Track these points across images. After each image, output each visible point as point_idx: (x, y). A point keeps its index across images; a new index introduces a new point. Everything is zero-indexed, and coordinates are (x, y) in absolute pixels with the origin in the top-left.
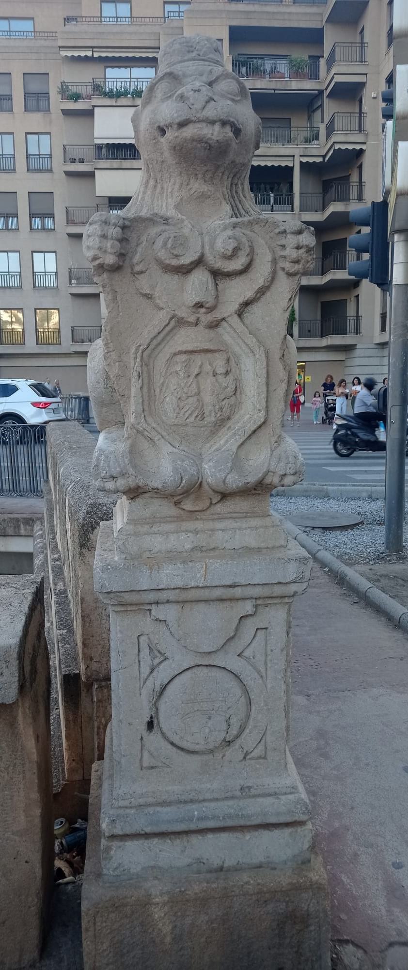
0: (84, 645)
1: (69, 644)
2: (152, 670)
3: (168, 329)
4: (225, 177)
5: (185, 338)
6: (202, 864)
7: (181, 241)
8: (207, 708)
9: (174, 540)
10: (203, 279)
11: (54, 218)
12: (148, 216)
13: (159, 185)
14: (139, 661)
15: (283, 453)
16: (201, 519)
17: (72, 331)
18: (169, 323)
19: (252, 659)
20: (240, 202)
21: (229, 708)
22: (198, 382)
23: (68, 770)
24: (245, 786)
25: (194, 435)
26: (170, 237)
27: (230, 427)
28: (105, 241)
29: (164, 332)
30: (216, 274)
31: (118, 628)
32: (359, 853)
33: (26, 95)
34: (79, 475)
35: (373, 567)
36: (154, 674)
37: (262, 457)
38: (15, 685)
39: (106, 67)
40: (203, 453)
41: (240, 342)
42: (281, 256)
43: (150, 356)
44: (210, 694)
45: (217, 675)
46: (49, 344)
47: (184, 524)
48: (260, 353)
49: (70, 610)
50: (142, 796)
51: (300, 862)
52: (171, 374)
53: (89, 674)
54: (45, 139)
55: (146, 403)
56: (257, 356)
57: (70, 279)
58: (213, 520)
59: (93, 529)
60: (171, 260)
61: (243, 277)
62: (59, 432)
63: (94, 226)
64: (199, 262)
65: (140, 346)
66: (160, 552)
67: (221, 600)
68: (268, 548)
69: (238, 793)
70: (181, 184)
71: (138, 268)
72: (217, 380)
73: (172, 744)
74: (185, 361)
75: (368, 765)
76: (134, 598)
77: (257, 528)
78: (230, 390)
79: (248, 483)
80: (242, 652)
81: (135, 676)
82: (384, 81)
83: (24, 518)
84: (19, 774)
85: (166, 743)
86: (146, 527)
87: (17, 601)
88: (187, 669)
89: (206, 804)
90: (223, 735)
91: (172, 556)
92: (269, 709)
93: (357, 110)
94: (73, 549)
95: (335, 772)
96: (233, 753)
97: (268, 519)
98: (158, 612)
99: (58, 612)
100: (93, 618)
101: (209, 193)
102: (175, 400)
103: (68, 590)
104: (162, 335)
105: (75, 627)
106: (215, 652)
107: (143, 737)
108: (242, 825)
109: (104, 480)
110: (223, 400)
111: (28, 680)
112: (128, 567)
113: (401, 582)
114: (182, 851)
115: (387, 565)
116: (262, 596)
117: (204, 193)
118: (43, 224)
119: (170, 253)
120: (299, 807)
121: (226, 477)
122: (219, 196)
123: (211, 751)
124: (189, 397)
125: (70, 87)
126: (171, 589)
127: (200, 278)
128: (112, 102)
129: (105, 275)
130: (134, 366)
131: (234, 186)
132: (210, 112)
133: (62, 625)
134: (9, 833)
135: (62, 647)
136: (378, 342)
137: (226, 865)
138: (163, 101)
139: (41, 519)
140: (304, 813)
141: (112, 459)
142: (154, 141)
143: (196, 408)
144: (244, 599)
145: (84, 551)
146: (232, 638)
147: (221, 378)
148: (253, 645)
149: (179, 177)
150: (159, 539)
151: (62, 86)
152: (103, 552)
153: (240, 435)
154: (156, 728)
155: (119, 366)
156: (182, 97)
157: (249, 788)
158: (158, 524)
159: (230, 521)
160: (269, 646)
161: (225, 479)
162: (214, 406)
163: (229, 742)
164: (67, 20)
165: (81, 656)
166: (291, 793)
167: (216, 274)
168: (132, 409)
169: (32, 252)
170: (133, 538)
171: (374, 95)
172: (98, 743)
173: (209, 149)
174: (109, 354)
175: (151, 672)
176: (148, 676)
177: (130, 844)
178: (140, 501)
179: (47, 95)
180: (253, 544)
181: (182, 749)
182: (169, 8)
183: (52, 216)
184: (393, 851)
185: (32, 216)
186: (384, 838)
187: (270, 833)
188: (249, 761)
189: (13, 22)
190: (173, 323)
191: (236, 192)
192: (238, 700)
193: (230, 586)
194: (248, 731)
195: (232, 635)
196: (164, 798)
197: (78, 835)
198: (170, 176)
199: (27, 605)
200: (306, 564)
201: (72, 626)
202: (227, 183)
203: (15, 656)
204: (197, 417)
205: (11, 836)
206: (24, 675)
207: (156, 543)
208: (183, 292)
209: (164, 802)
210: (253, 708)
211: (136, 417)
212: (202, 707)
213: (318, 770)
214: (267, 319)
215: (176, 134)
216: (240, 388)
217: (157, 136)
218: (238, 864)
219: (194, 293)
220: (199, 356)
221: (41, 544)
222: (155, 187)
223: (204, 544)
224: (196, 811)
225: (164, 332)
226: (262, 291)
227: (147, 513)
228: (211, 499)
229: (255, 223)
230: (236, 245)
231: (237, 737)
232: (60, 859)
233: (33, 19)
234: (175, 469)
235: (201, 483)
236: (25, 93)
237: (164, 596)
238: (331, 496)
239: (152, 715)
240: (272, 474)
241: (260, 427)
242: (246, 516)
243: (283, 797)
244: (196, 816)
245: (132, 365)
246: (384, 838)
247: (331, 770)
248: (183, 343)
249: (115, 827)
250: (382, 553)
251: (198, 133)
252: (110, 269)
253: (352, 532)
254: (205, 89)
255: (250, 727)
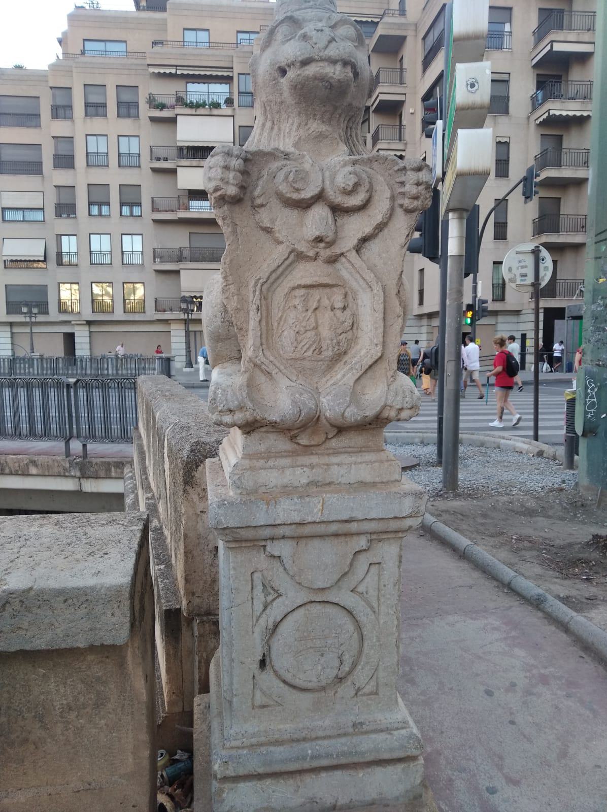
0: (187, 580)
1: (168, 579)
2: (265, 608)
3: (287, 262)
4: (342, 119)
5: (305, 273)
6: (315, 804)
7: (302, 176)
8: (320, 646)
9: (290, 475)
10: (323, 213)
11: (141, 206)
12: (269, 150)
13: (276, 127)
14: (252, 599)
15: (399, 387)
16: (316, 454)
17: (156, 302)
18: (288, 257)
19: (365, 595)
20: (354, 146)
21: (342, 644)
22: (316, 315)
23: (168, 702)
24: (357, 722)
25: (310, 369)
26: (291, 171)
27: (346, 362)
28: (227, 172)
29: (283, 266)
30: (337, 210)
31: (231, 564)
32: (454, 778)
33: (119, 104)
34: (177, 418)
35: (434, 503)
36: (268, 611)
37: (379, 391)
38: (127, 626)
39: (187, 83)
40: (319, 387)
41: (357, 276)
42: (400, 193)
43: (268, 290)
45: (331, 611)
46: (135, 312)
47: (299, 458)
48: (377, 289)
49: (167, 546)
50: (254, 735)
51: (412, 798)
52: (289, 308)
53: (191, 609)
54: (134, 141)
55: (264, 336)
56: (375, 291)
57: (154, 258)
58: (329, 455)
59: (197, 467)
60: (292, 193)
61: (361, 214)
62: (150, 383)
63: (216, 158)
64: (320, 197)
65: (259, 279)
66: (276, 486)
67: (336, 535)
68: (382, 482)
69: (351, 730)
70: (300, 125)
71: (259, 201)
72: (334, 315)
73: (285, 682)
74: (304, 295)
75: (452, 689)
76: (250, 534)
77: (372, 462)
78: (347, 325)
79: (367, 417)
80: (356, 587)
82: (420, 100)
83: (115, 462)
84: (128, 716)
86: (262, 462)
87: (125, 538)
88: (301, 606)
89: (319, 742)
90: (335, 672)
91: (288, 491)
92: (381, 645)
93: (398, 123)
94: (173, 487)
95: (423, 698)
96: (346, 690)
97: (382, 453)
98: (275, 548)
99: (155, 548)
100: (196, 554)
101: (327, 133)
102: (293, 334)
103: (164, 527)
104: (281, 269)
105: (173, 562)
106: (329, 588)
107: (256, 676)
108: (356, 762)
109: (221, 414)
110: (341, 334)
111: (138, 619)
112: (244, 502)
113: (460, 516)
114: (295, 790)
115: (446, 501)
117: (322, 133)
118: (131, 212)
119: (291, 186)
120: (411, 742)
121: (345, 411)
122: (336, 136)
123: (323, 689)
124: (306, 331)
125: (156, 98)
126: (287, 524)
127: (319, 214)
128: (192, 111)
129: (226, 207)
130: (253, 300)
131: (349, 129)
132: (333, 51)
133: (160, 560)
134: (116, 777)
135: (161, 582)
136: (417, 313)
137: (339, 804)
138: (283, 43)
139: (131, 463)
140: (416, 748)
141: (229, 392)
142: (274, 82)
143: (314, 342)
144: (359, 534)
145: (188, 488)
146: (345, 574)
147: (338, 313)
148: (366, 581)
149: (297, 117)
150: (275, 473)
151: (150, 97)
152: (216, 488)
153: (357, 369)
154: (268, 667)
155: (238, 299)
156: (305, 37)
157: (361, 724)
158: (274, 459)
159: (346, 455)
161: (344, 413)
162: (332, 340)
164: (155, 43)
165: (182, 591)
166: (403, 728)
167: (337, 210)
168: (250, 342)
169: (122, 234)
170: (249, 472)
171: (412, 111)
172: (200, 677)
173: (330, 89)
174: (228, 287)
175: (264, 610)
176: (261, 614)
177: (243, 786)
178: (256, 436)
179: (136, 105)
180: (368, 478)
182: (241, 36)
183: (139, 204)
184: (485, 775)
185: (122, 204)
186: (475, 762)
187: (383, 769)
188: (361, 697)
189: (108, 44)
190: (292, 257)
191: (351, 136)
192: (351, 637)
193: (346, 521)
194: (360, 667)
195: (346, 570)
196: (276, 737)
197: (179, 766)
198: (289, 117)
199: (137, 542)
200: (421, 499)
201: (170, 561)
202: (343, 125)
203: (127, 595)
204: (314, 351)
205: (119, 780)
206: (134, 614)
207: (272, 478)
208: (302, 227)
209: (277, 741)
210: (366, 644)
211: (254, 350)
212: (315, 644)
213: (406, 696)
214: (384, 255)
215: (299, 72)
216: (356, 323)
217: (277, 77)
218: (351, 802)
219: (314, 227)
220: (318, 291)
221: (131, 485)
222: (272, 128)
223: (320, 479)
224: (309, 749)
225: (283, 266)
226: (380, 227)
227: (262, 448)
228: (327, 433)
229: (374, 160)
230: (356, 180)
231: (349, 673)
232: (161, 792)
233: (125, 42)
234: (294, 402)
235: (319, 416)
236: (118, 102)
237: (281, 531)
238: (388, 441)
240: (389, 408)
241: (376, 362)
242: (361, 450)
243: (395, 733)
244: (310, 755)
245: (251, 298)
246: (475, 762)
247: (418, 695)
248: (302, 277)
249: (228, 769)
250: (440, 491)
251: (321, 71)
252: (231, 201)
253: (410, 473)
254: (327, 31)
255: (362, 663)
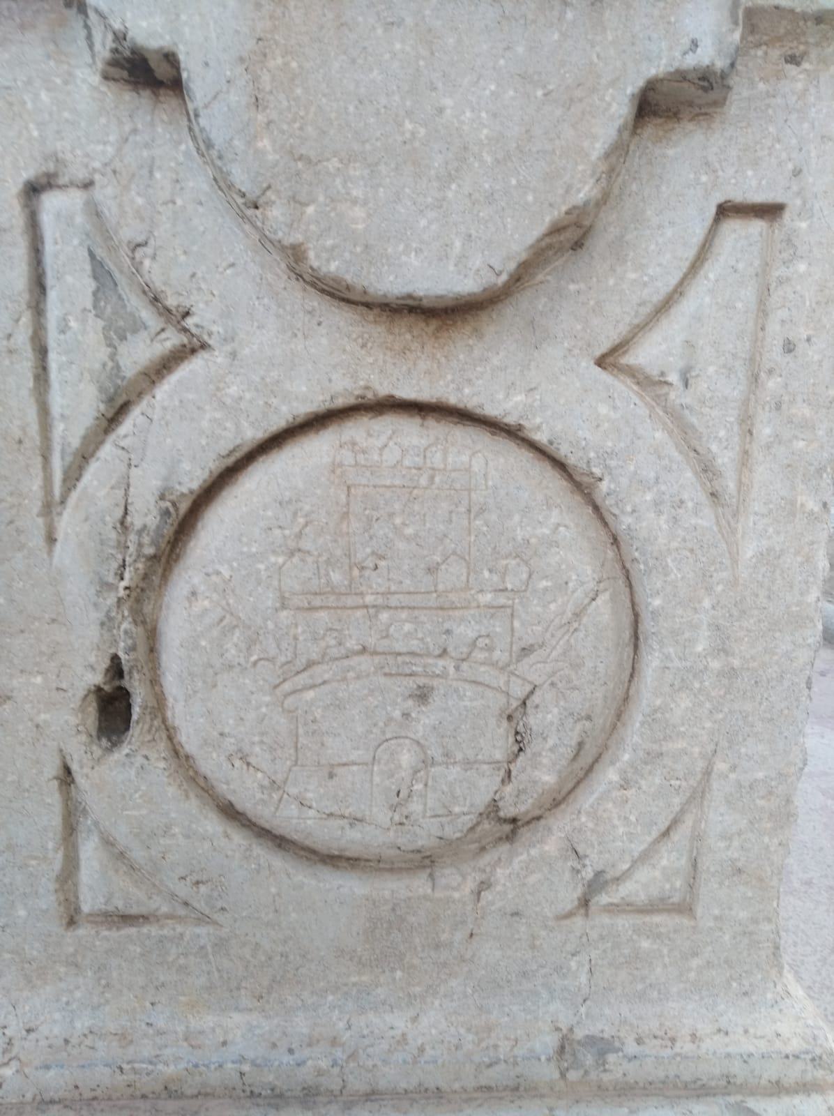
8: (414, 645)
21: (526, 651)
24: (579, 1034)
44: (432, 570)
45: (478, 465)
73: (230, 812)
75: (809, 883)
81: (17, 433)
85: (193, 804)
107: (74, 767)
116: (348, 854)
157: (602, 1047)
160: (774, 327)
163: (514, 820)
181: (281, 842)
188: (606, 920)
210: (651, 662)
231: (558, 800)
239: (115, 659)
